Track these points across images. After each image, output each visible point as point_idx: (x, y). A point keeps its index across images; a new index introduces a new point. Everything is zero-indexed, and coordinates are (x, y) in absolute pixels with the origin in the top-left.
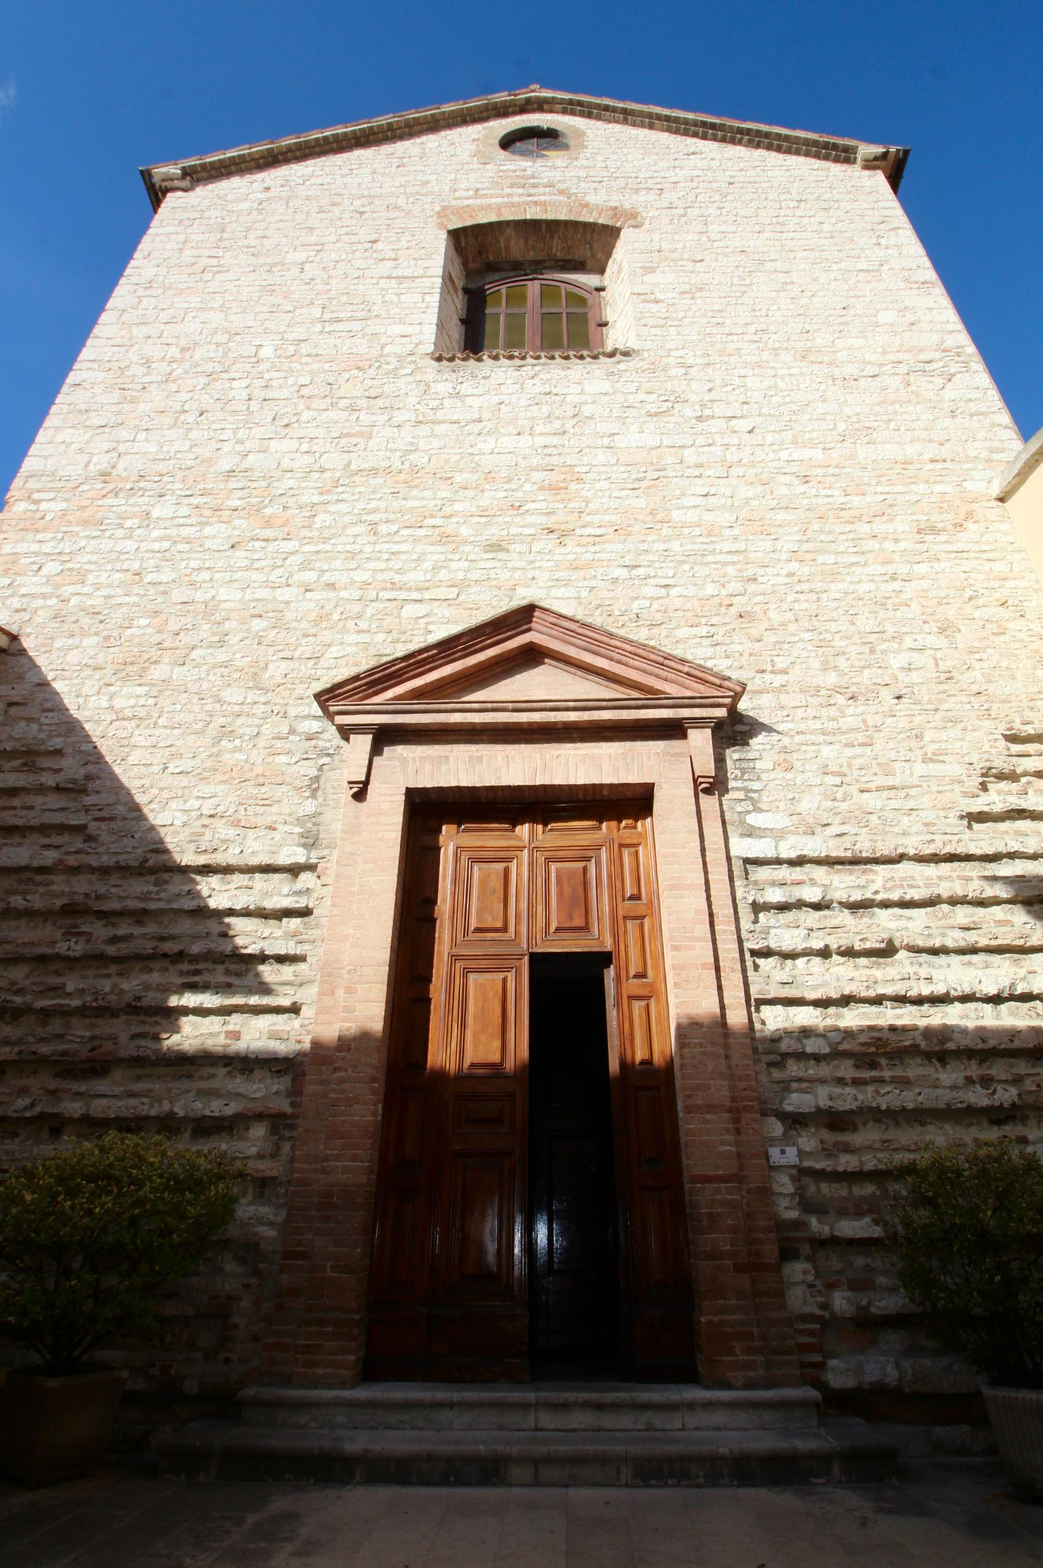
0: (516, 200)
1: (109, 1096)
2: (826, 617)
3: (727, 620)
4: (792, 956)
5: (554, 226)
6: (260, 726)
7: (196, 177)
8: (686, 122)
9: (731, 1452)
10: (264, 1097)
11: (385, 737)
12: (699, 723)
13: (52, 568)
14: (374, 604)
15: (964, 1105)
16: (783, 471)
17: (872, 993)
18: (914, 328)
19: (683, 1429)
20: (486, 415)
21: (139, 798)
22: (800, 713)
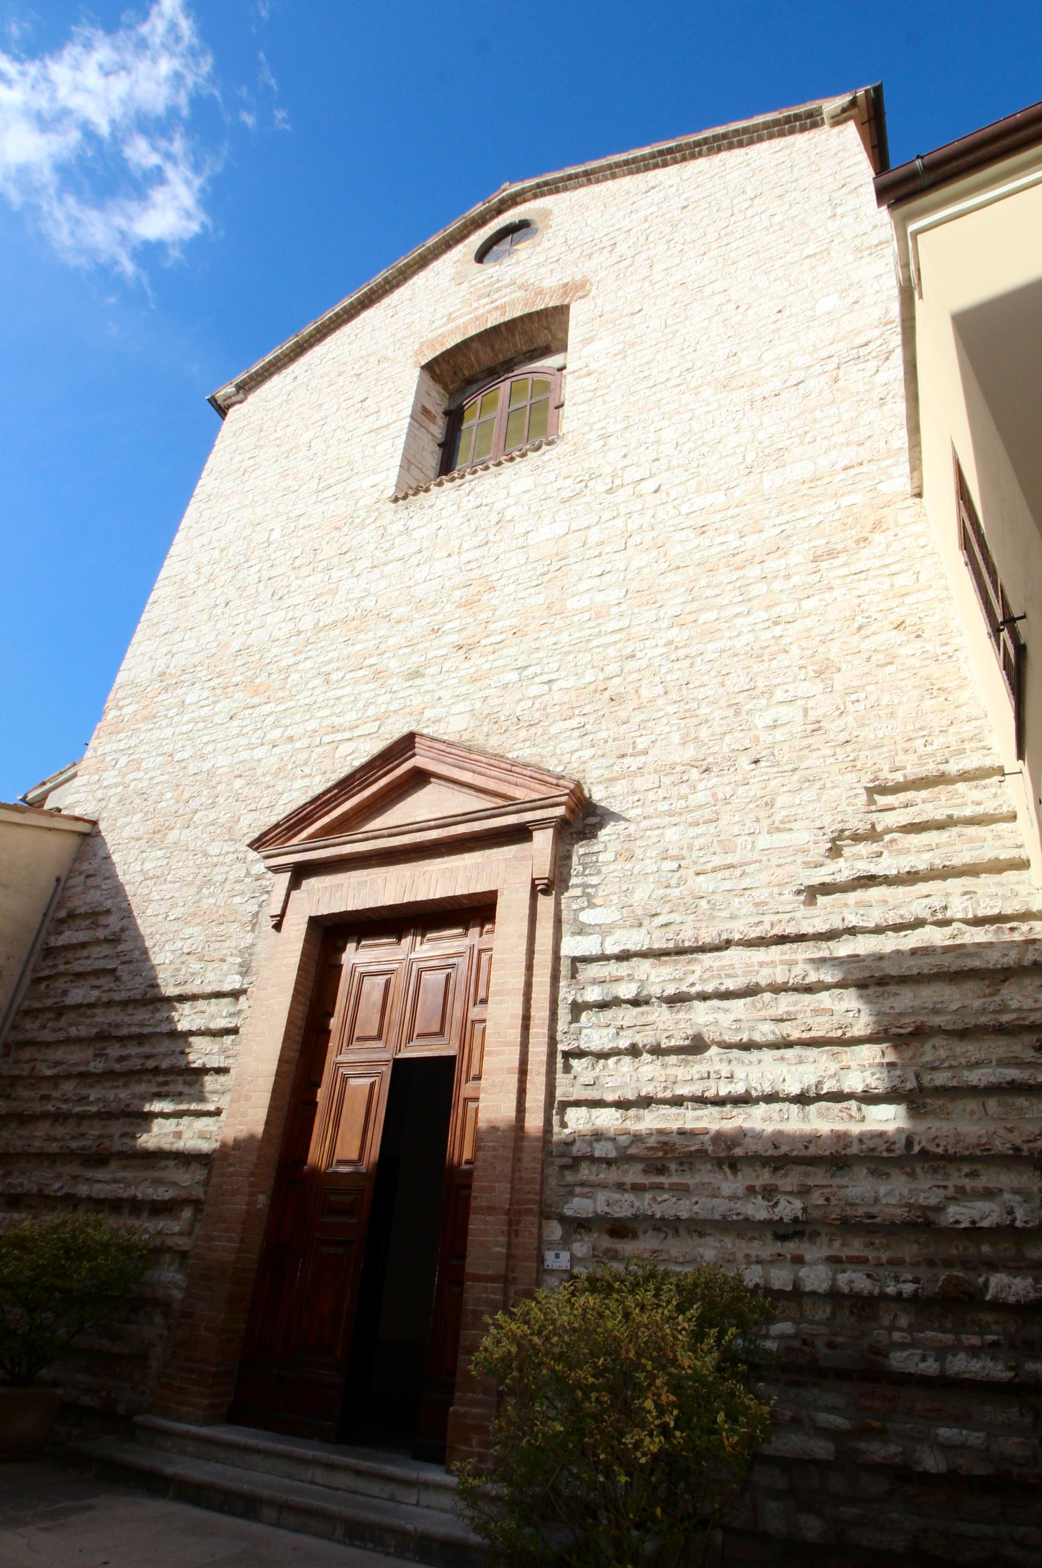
0: (480, 311)
1: (103, 1183)
2: (697, 684)
3: (599, 706)
4: (602, 1055)
5: (511, 325)
6: (228, 872)
7: (246, 387)
8: (644, 158)
9: (416, 1530)
10: (190, 1186)
11: (301, 873)
12: (542, 824)
13: (123, 761)
14: (318, 749)
15: (740, 1217)
16: (682, 526)
17: (668, 1094)
18: (857, 307)
19: (417, 1505)
20: (425, 545)
21: (149, 943)
22: (651, 796)
